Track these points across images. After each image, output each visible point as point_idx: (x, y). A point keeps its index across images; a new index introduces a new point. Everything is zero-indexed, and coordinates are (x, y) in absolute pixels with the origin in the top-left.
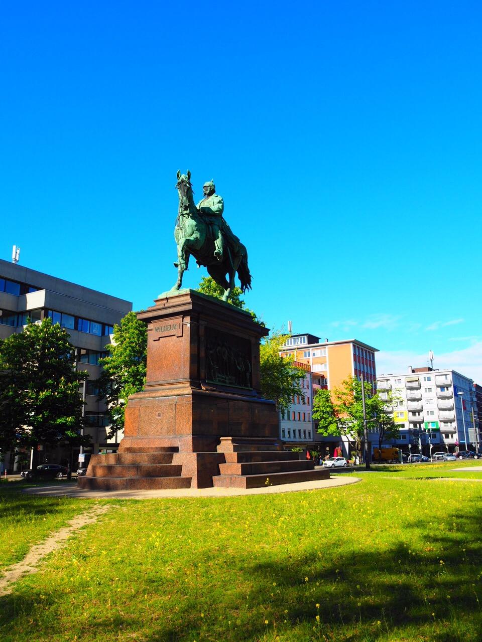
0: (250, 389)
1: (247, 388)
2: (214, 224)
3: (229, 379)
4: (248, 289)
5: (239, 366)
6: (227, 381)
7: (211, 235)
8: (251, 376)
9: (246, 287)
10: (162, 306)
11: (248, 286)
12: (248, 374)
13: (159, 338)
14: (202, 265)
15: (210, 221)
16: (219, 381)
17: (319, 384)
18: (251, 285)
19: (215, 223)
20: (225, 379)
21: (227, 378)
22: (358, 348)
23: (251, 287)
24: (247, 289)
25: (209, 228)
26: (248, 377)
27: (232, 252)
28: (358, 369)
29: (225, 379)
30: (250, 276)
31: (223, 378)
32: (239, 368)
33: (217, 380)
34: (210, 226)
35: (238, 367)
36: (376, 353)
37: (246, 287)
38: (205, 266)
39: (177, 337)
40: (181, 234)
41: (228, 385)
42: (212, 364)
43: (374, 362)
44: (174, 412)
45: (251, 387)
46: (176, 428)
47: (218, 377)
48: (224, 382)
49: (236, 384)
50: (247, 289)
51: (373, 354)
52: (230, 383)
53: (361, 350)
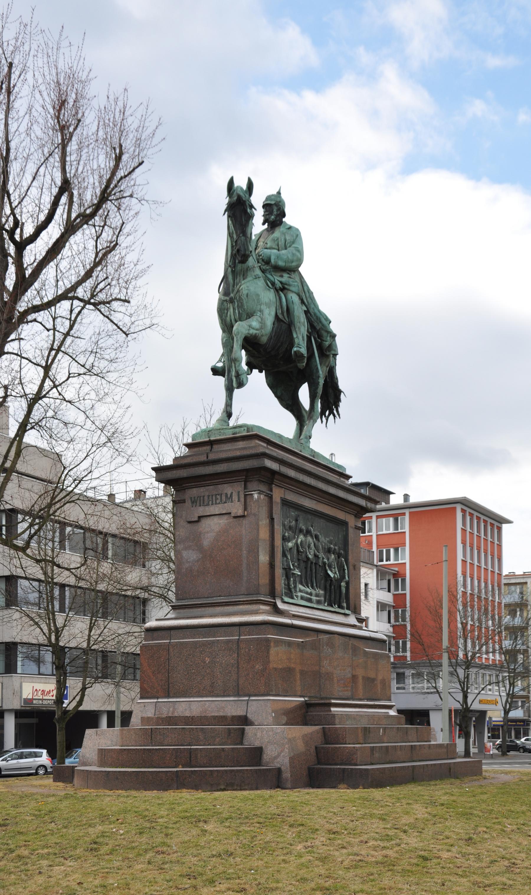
0: (347, 612)
1: (342, 611)
2: (288, 290)
3: (317, 595)
4: (334, 416)
5: (331, 571)
6: (314, 598)
7: (285, 314)
8: (347, 588)
9: (331, 412)
10: (203, 458)
11: (335, 412)
12: (343, 584)
13: (200, 517)
14: (256, 368)
15: (281, 282)
16: (302, 598)
17: (389, 591)
18: (340, 409)
19: (292, 288)
20: (311, 594)
21: (314, 592)
22: (471, 515)
23: (339, 415)
24: (332, 416)
25: (280, 298)
26: (344, 590)
27: (320, 347)
28: (469, 561)
29: (311, 594)
30: (340, 392)
31: (307, 593)
32: (332, 575)
33: (299, 598)
34: (281, 293)
35: (329, 572)
36: (505, 526)
37: (331, 412)
38: (261, 371)
39: (235, 517)
40: (232, 310)
41: (315, 606)
42: (292, 567)
43: (500, 546)
44: (236, 655)
45: (348, 608)
46: (240, 683)
47: (301, 591)
48: (310, 600)
49: (326, 604)
50: (331, 416)
51: (500, 529)
52: (318, 602)
53: (475, 521)
